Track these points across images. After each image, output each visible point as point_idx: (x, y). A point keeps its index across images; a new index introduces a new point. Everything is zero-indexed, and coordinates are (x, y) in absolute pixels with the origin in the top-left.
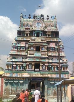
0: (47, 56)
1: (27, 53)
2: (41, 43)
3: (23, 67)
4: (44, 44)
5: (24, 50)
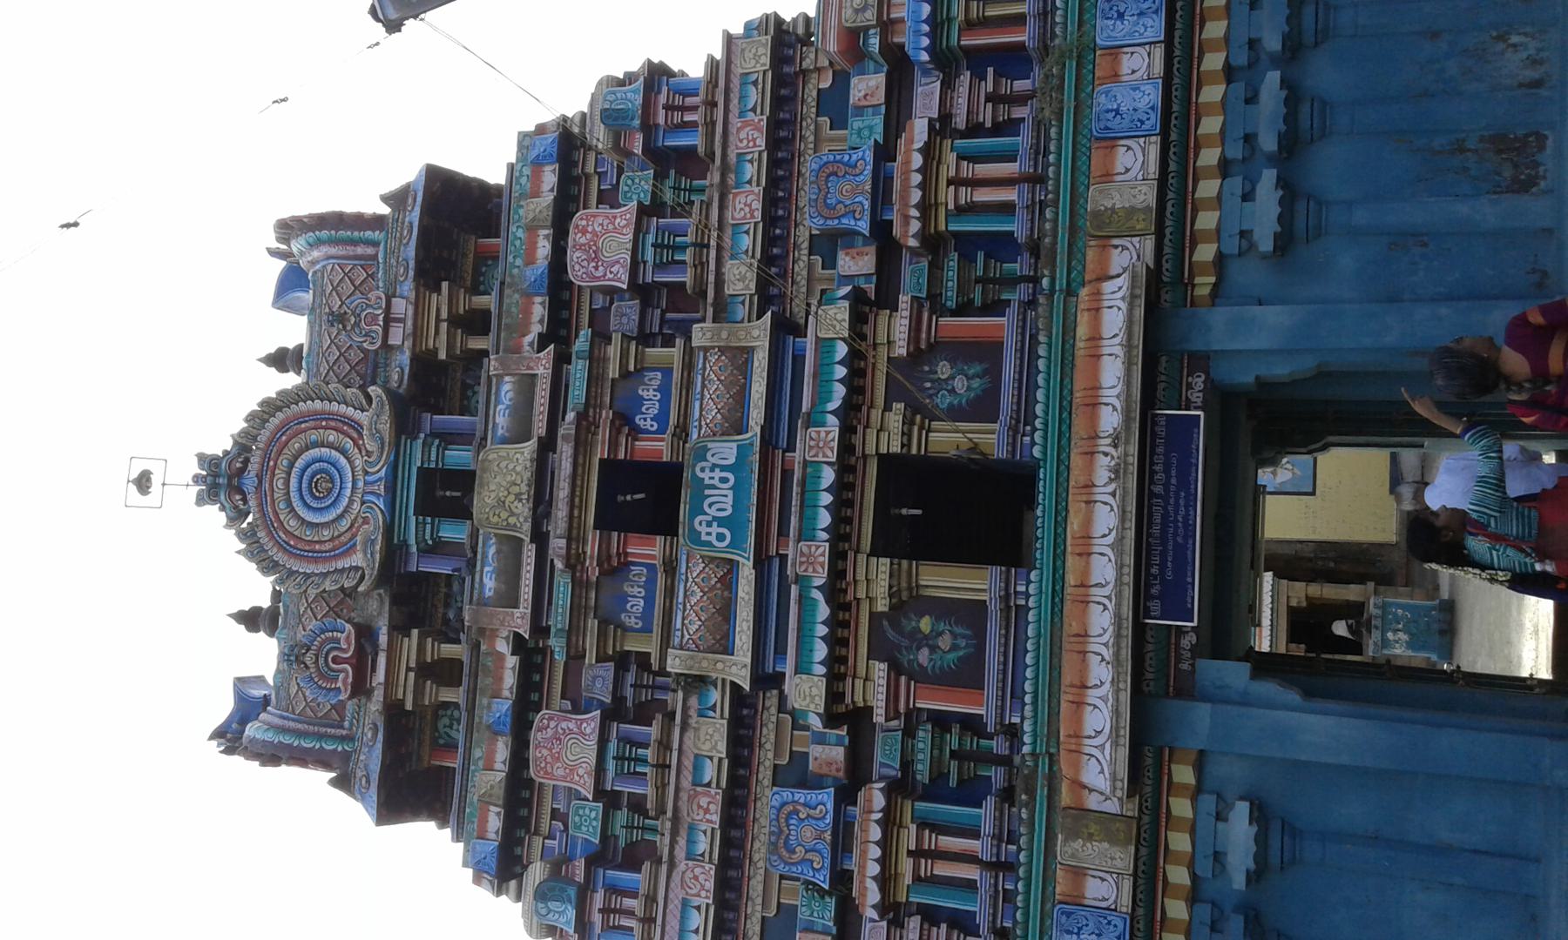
0: (759, 334)
1: (696, 683)
2: (547, 445)
3: (936, 790)
4: (577, 392)
5: (654, 731)
